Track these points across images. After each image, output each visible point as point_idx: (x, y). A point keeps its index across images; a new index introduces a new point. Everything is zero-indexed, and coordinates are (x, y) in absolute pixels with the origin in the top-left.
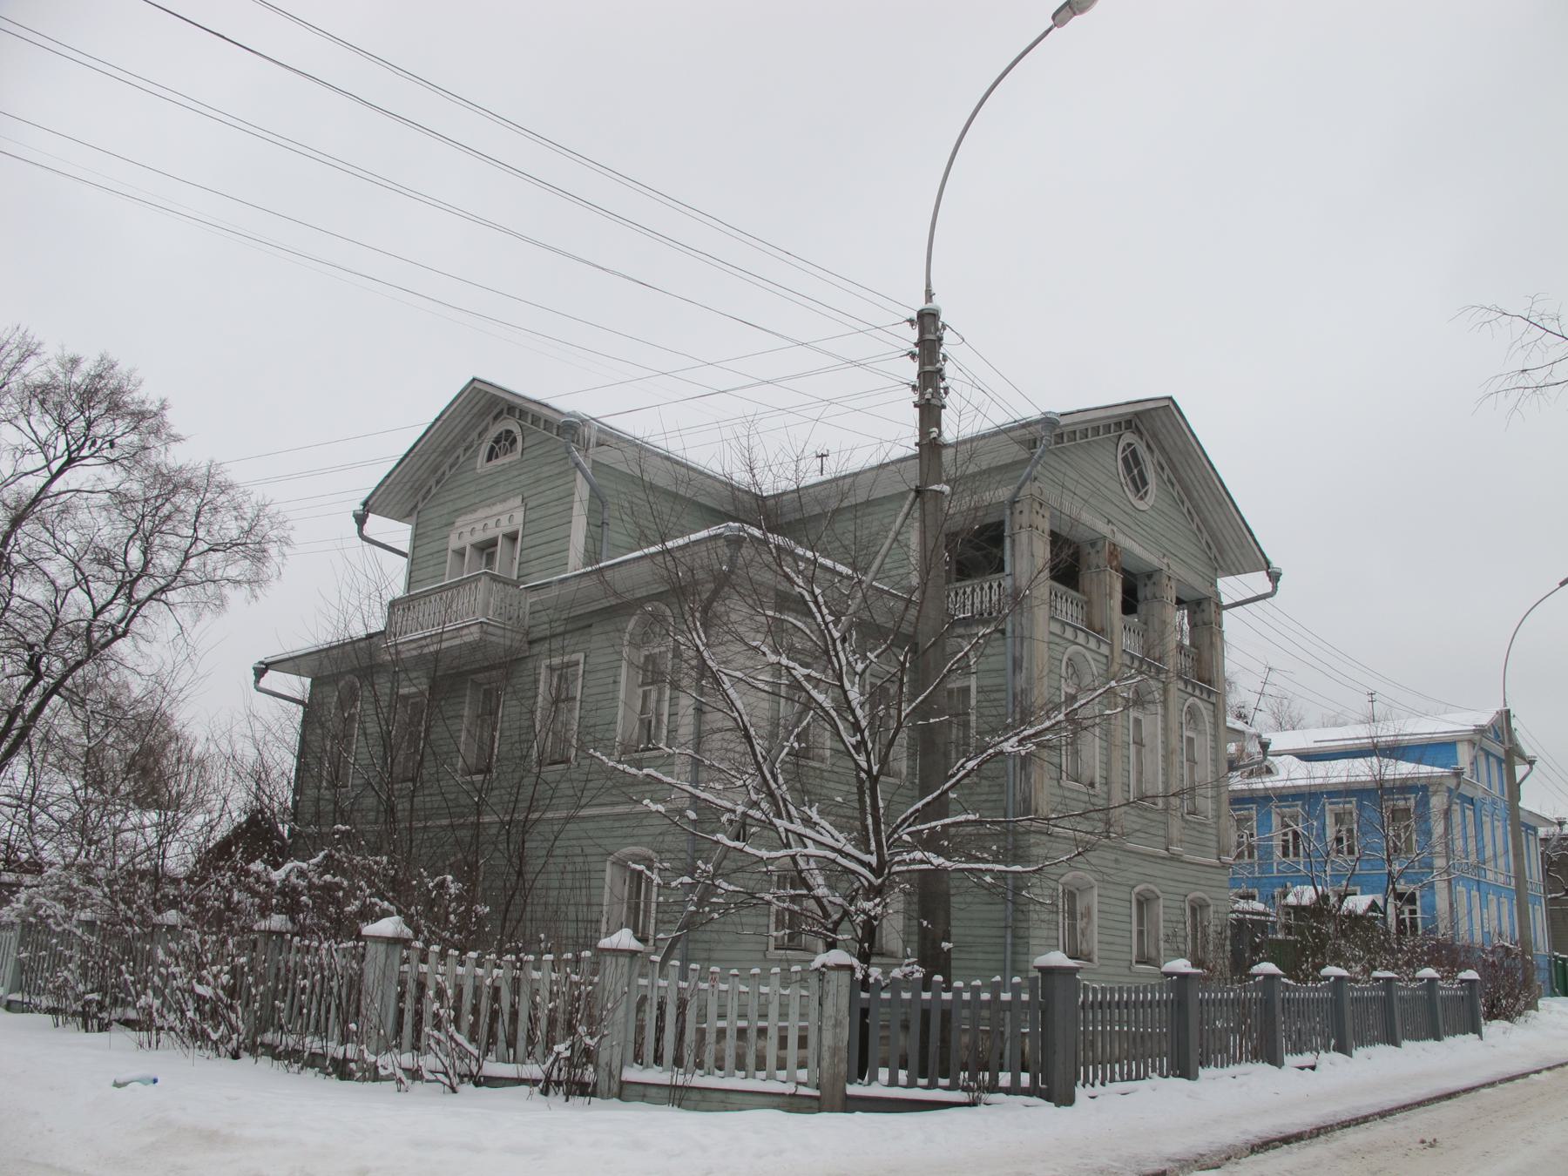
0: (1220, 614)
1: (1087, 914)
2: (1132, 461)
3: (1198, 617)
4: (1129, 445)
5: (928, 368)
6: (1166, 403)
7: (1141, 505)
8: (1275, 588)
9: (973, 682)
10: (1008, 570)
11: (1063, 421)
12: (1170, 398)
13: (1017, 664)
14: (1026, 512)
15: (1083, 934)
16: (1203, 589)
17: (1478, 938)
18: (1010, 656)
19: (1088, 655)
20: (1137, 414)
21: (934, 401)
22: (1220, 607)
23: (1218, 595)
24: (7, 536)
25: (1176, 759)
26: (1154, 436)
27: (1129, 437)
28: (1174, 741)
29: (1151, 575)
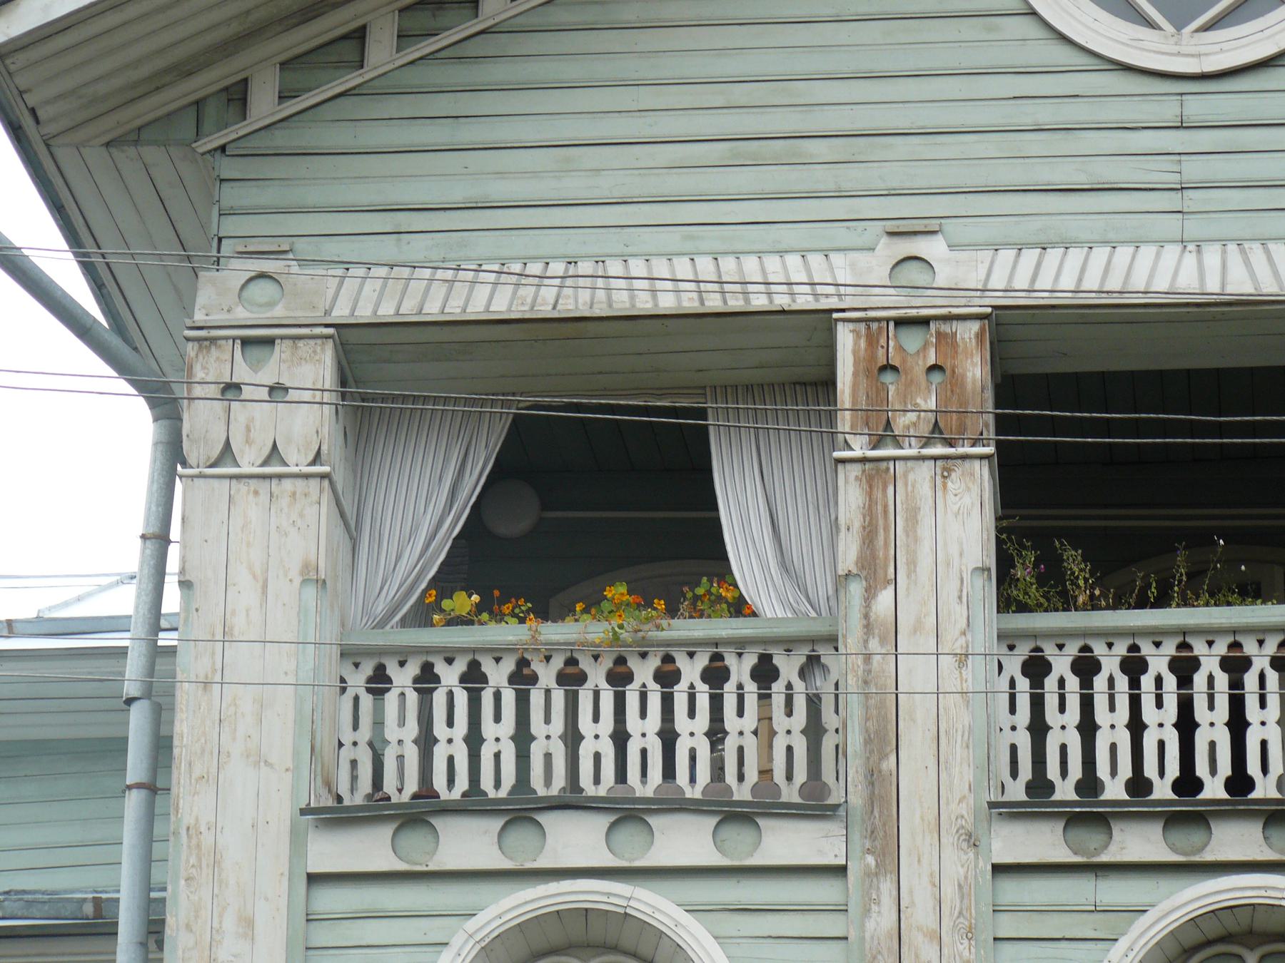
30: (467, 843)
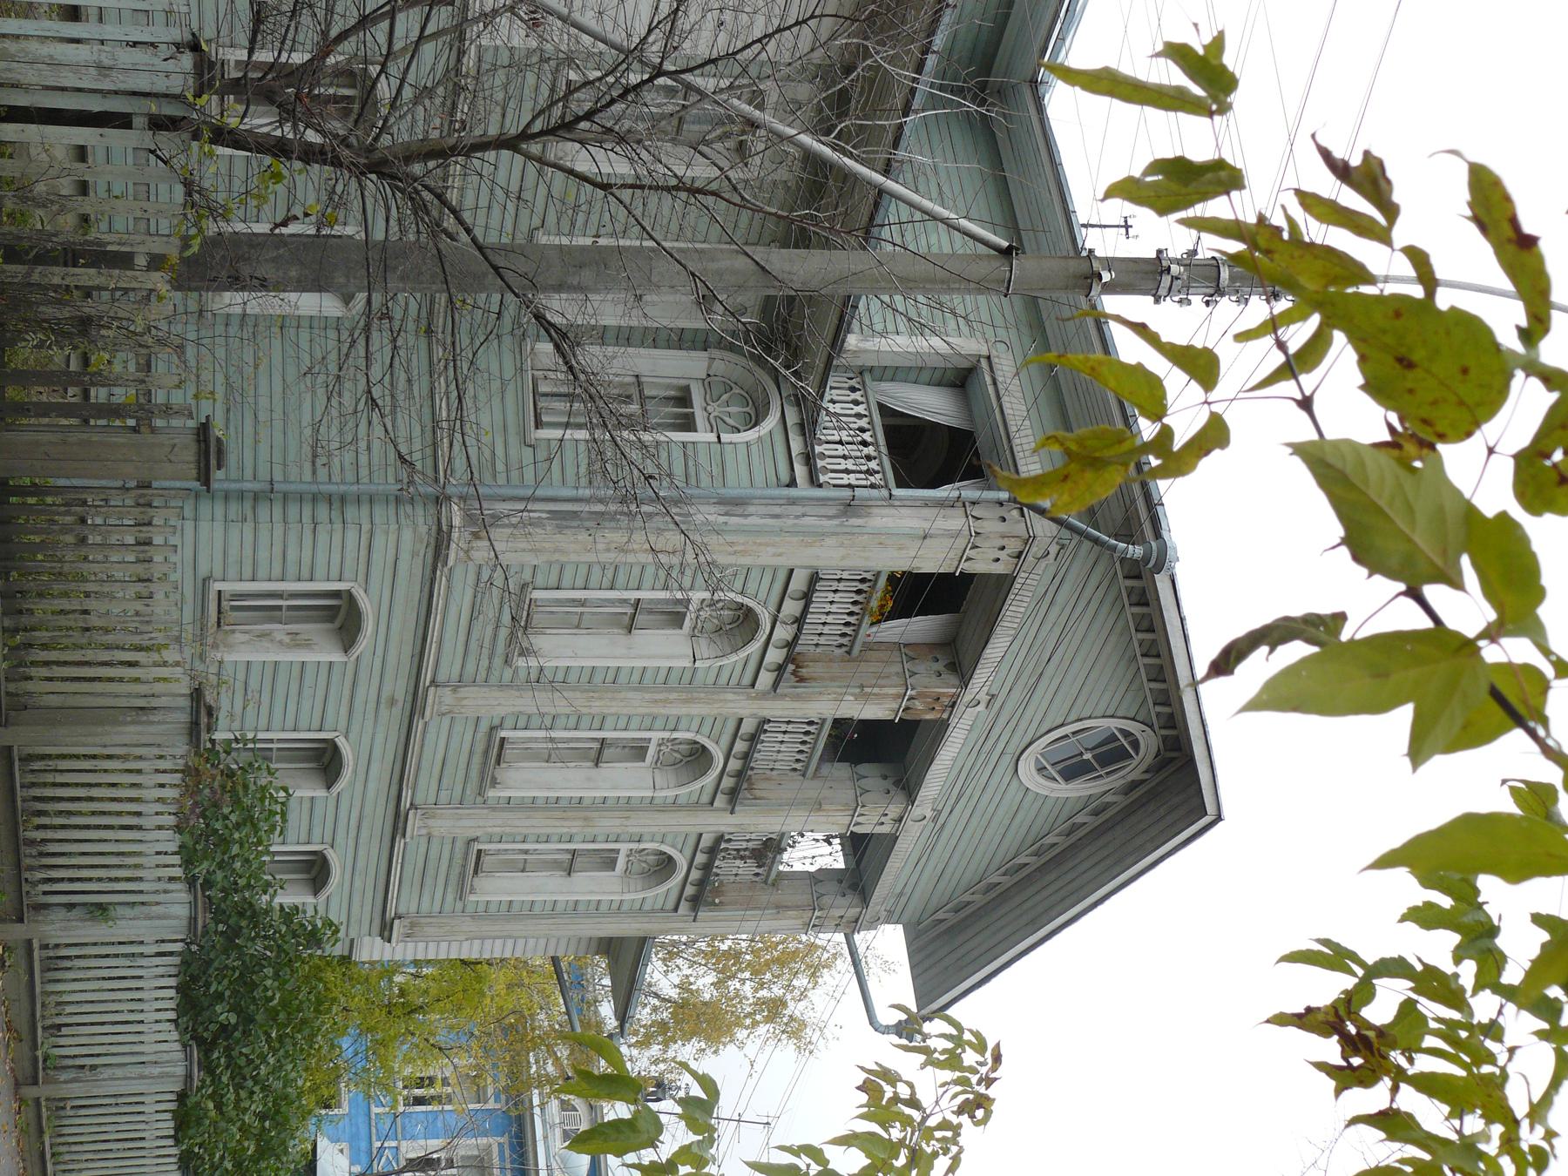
0: (837, 928)
1: (297, 642)
2: (1112, 753)
3: (833, 887)
4: (1135, 744)
5: (1225, 274)
6: (1210, 808)
7: (1027, 768)
8: (885, 1030)
9: (703, 436)
10: (897, 492)
11: (1161, 581)
12: (1219, 818)
13: (734, 504)
14: (1002, 527)
15: (262, 635)
16: (883, 890)
17: (173, 982)
18: (750, 492)
19: (755, 647)
20: (1191, 761)
21: (1166, 280)
22: (851, 927)
23: (873, 924)
24: (1555, 1085)
25: (574, 826)
26: (1152, 795)
27: (1149, 742)
28: (608, 824)
29: (908, 788)
30: (791, 608)
